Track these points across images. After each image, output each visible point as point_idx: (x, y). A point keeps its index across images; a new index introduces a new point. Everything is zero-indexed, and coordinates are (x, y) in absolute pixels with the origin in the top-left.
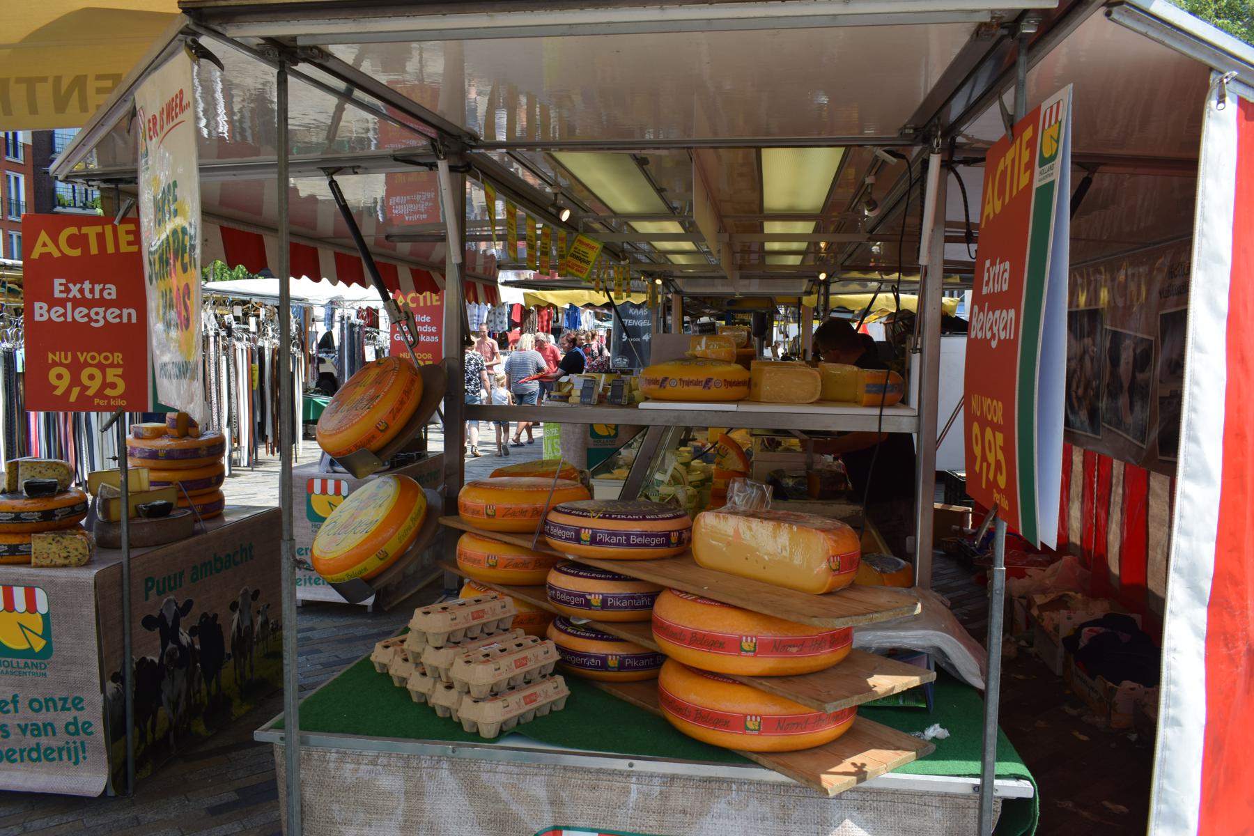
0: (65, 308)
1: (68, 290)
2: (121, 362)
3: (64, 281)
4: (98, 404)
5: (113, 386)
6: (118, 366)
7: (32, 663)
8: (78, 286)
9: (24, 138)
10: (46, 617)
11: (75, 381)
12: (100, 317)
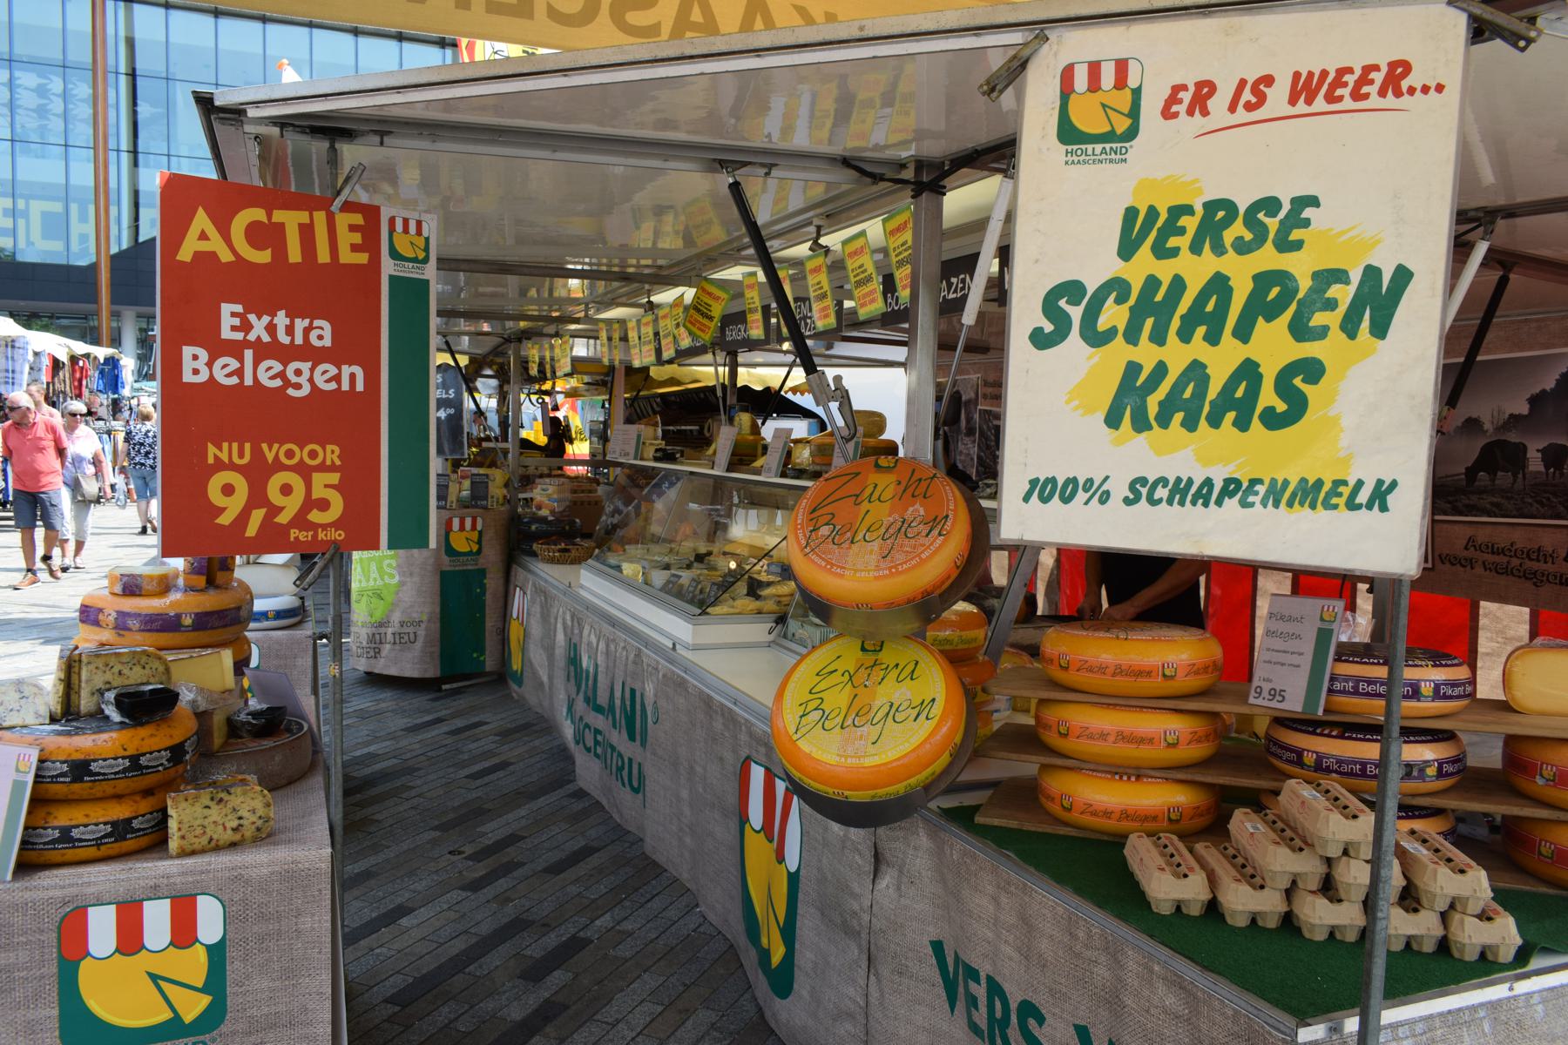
0: (241, 359)
1: (246, 327)
2: (338, 462)
3: (239, 308)
4: (297, 538)
5: (324, 505)
6: (332, 469)
10: (217, 952)
11: (257, 497)
12: (303, 380)
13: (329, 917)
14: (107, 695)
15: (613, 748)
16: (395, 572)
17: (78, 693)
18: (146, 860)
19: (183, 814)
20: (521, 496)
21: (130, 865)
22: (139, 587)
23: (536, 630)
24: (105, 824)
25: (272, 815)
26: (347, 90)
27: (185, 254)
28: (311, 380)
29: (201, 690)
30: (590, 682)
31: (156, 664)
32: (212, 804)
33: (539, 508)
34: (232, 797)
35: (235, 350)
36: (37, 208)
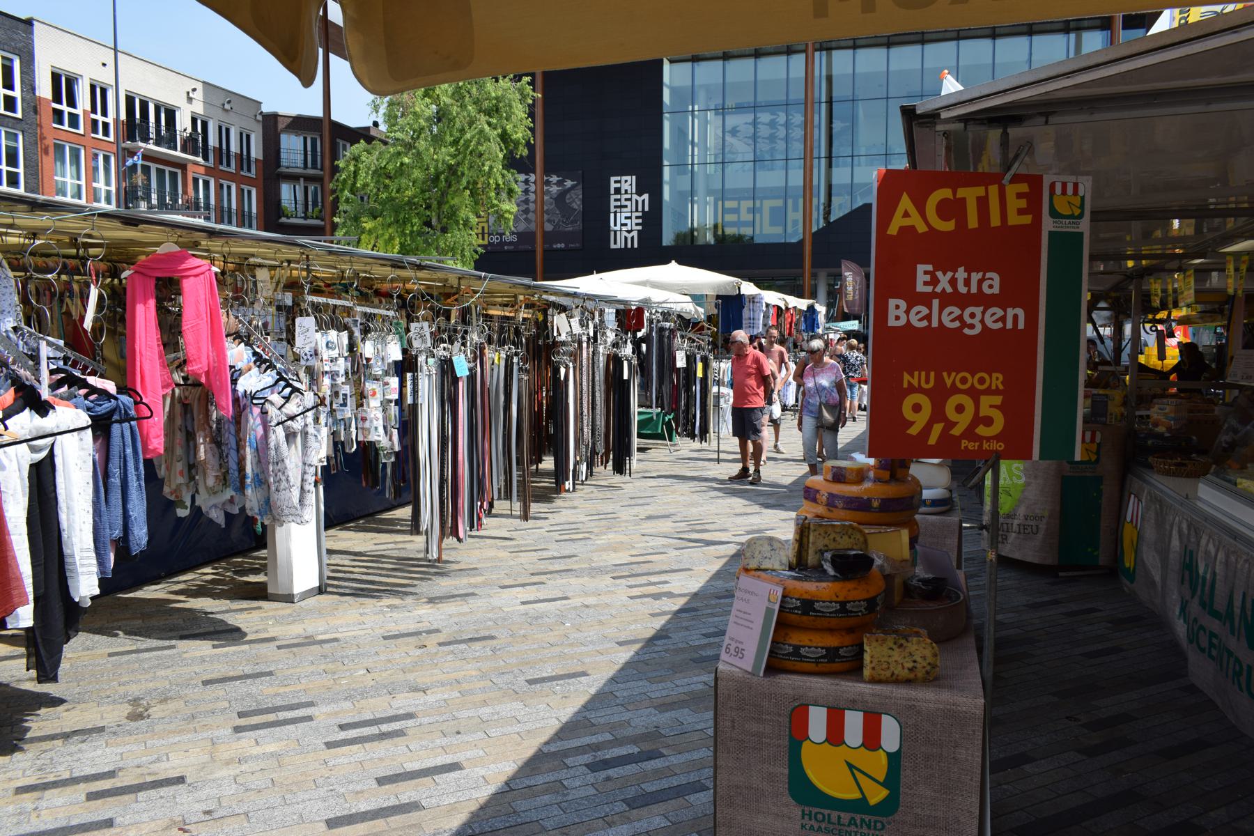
0: (930, 307)
1: (934, 281)
2: (1001, 387)
3: (930, 268)
4: (966, 447)
5: (988, 421)
6: (996, 392)
7: (863, 820)
8: (950, 274)
9: (256, 153)
10: (894, 758)
11: (938, 414)
12: (976, 321)
13: (980, 754)
14: (826, 554)
15: (1230, 654)
16: (1021, 474)
17: (807, 551)
18: (848, 680)
19: (874, 651)
20: (1138, 413)
21: (837, 681)
22: (843, 476)
23: (1150, 534)
24: (822, 648)
25: (938, 663)
26: (1023, 83)
27: (893, 230)
28: (982, 321)
29: (887, 559)
30: (1207, 588)
31: (858, 536)
32: (894, 647)
33: (1156, 425)
34: (909, 644)
35: (926, 300)
36: (768, 204)
